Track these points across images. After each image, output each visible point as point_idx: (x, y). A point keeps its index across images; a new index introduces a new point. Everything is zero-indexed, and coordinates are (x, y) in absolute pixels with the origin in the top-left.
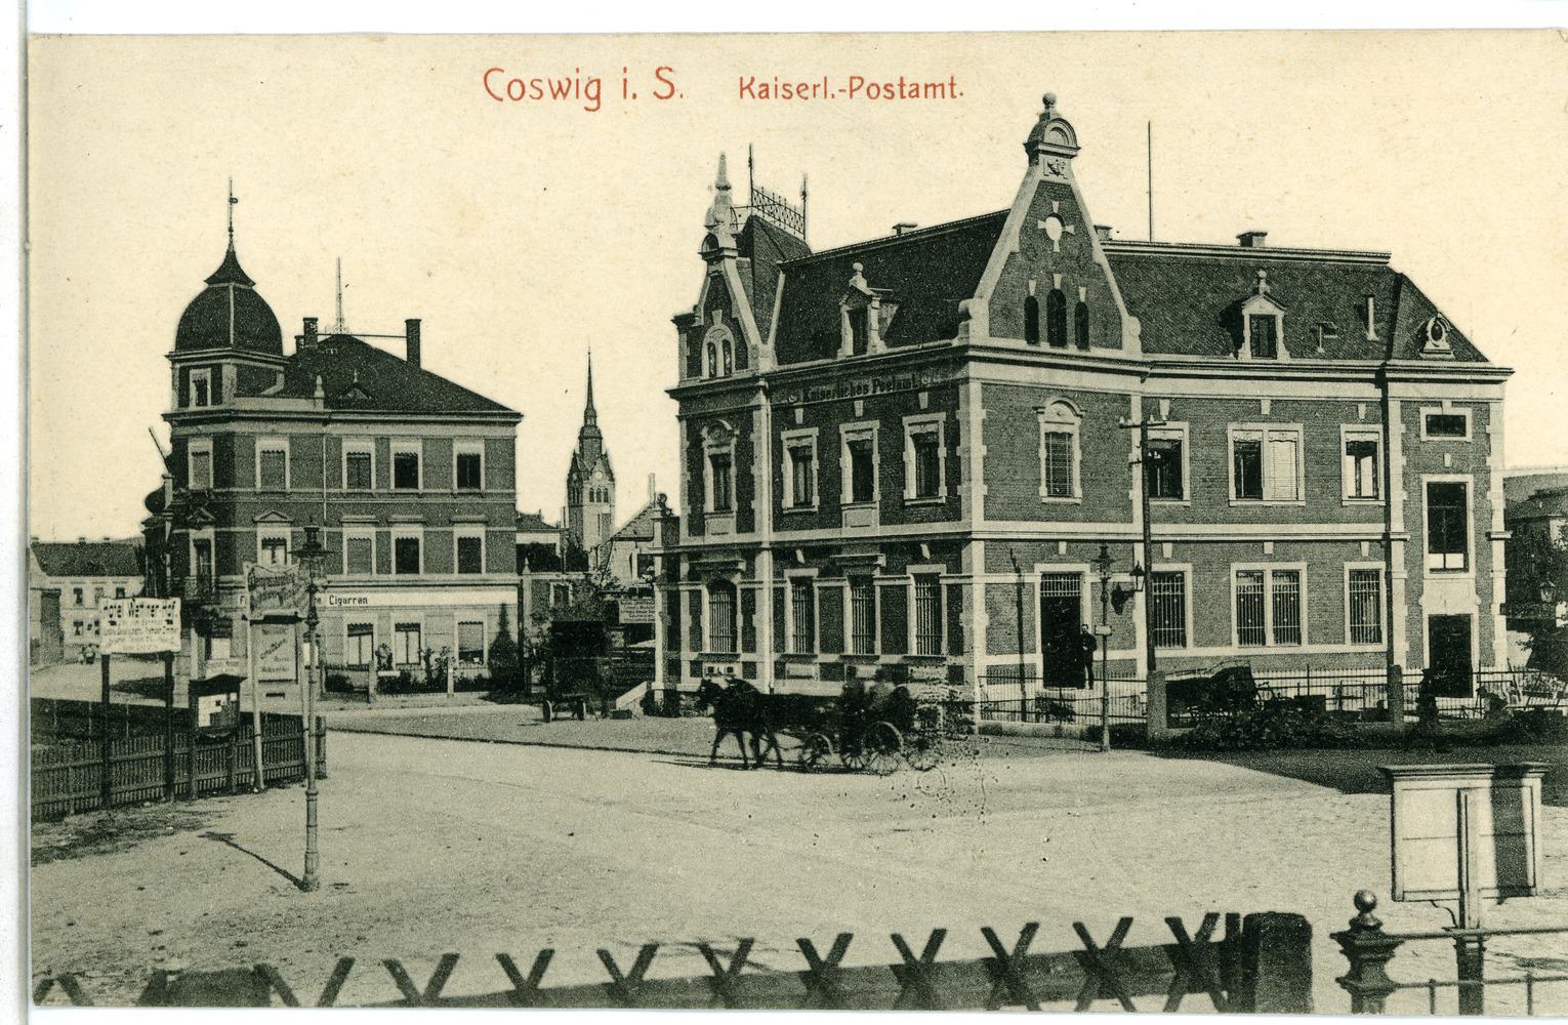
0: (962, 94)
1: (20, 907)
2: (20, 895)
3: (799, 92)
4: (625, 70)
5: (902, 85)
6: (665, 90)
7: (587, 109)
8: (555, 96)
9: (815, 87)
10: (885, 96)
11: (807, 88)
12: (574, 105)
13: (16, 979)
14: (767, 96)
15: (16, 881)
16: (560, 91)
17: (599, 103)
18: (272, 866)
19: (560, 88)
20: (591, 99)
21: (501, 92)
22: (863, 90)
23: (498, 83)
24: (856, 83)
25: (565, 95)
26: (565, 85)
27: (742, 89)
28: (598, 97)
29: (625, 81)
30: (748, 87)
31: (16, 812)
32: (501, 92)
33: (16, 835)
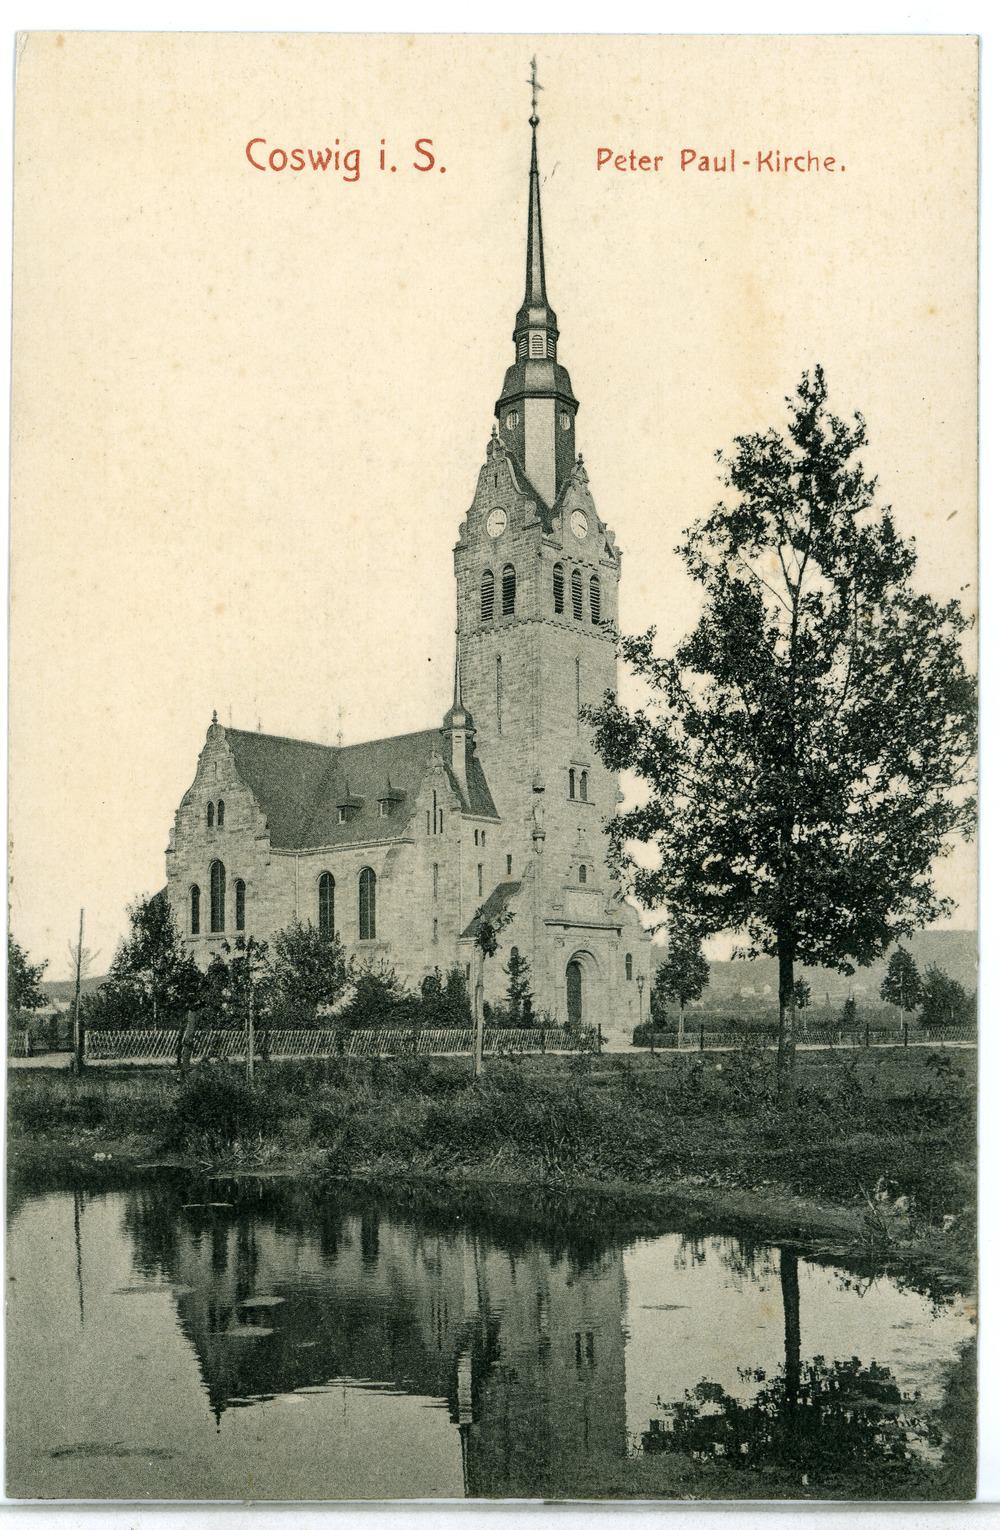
0: (443, 170)
1: (894, 1510)
2: (882, 1511)
3: (825, 165)
4: (383, 142)
5: (632, 158)
6: (424, 161)
7: (346, 179)
8: (315, 167)
9: (656, 159)
10: (292, 166)
11: (649, 161)
12: (333, 175)
13: (964, 1515)
14: (707, 169)
15: (868, 1514)
16: (320, 163)
17: (358, 174)
18: (509, 867)
19: (320, 159)
20: (351, 169)
21: (265, 162)
22: (612, 161)
23: (261, 153)
24: (688, 156)
25: (324, 167)
26: (325, 156)
27: (760, 162)
28: (357, 167)
29: (382, 152)
30: (766, 161)
31: (801, 1515)
32: (265, 162)
33: (823, 1514)
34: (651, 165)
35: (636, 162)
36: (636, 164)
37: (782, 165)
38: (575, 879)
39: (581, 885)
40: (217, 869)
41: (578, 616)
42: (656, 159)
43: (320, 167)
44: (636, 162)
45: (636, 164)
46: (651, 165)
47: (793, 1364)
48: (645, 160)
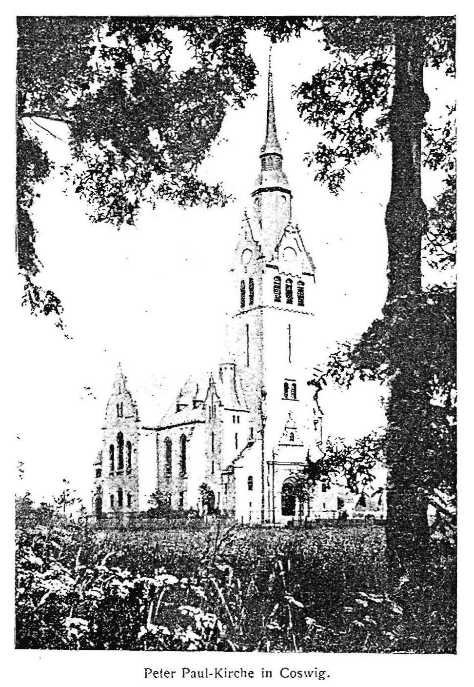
34: (170, 675)
35: (163, 674)
36: (163, 675)
37: (228, 675)
38: (286, 440)
39: (292, 443)
40: (120, 436)
41: (290, 302)
42: (172, 672)
43: (433, 168)
44: (163, 674)
45: (163, 675)
46: (170, 675)
48: (167, 672)
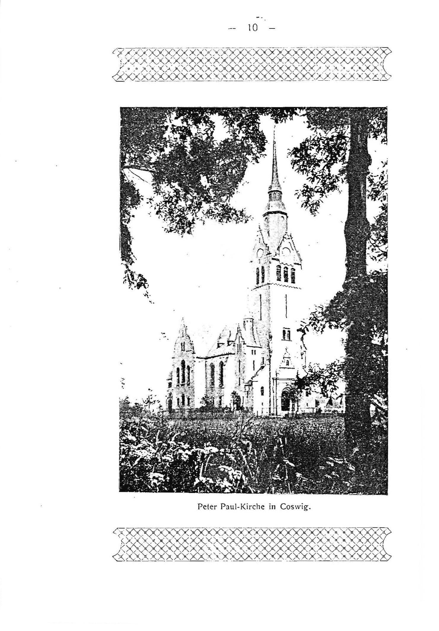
5: (208, 506)
34: (213, 508)
35: (209, 507)
36: (209, 508)
37: (249, 508)
38: (284, 365)
39: (287, 367)
45: (209, 508)
46: (213, 508)
47: (294, 165)
